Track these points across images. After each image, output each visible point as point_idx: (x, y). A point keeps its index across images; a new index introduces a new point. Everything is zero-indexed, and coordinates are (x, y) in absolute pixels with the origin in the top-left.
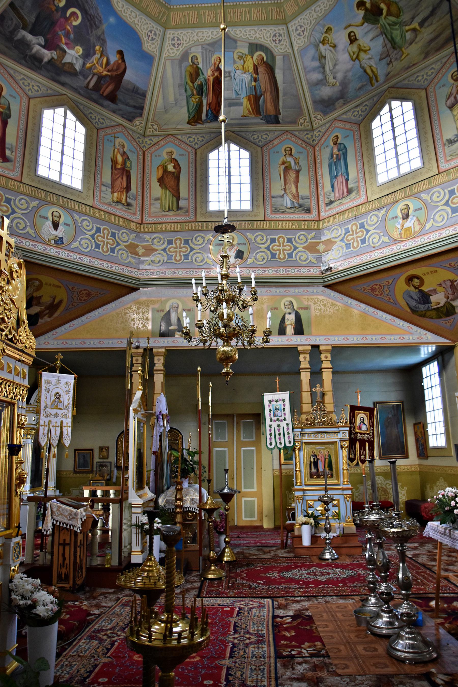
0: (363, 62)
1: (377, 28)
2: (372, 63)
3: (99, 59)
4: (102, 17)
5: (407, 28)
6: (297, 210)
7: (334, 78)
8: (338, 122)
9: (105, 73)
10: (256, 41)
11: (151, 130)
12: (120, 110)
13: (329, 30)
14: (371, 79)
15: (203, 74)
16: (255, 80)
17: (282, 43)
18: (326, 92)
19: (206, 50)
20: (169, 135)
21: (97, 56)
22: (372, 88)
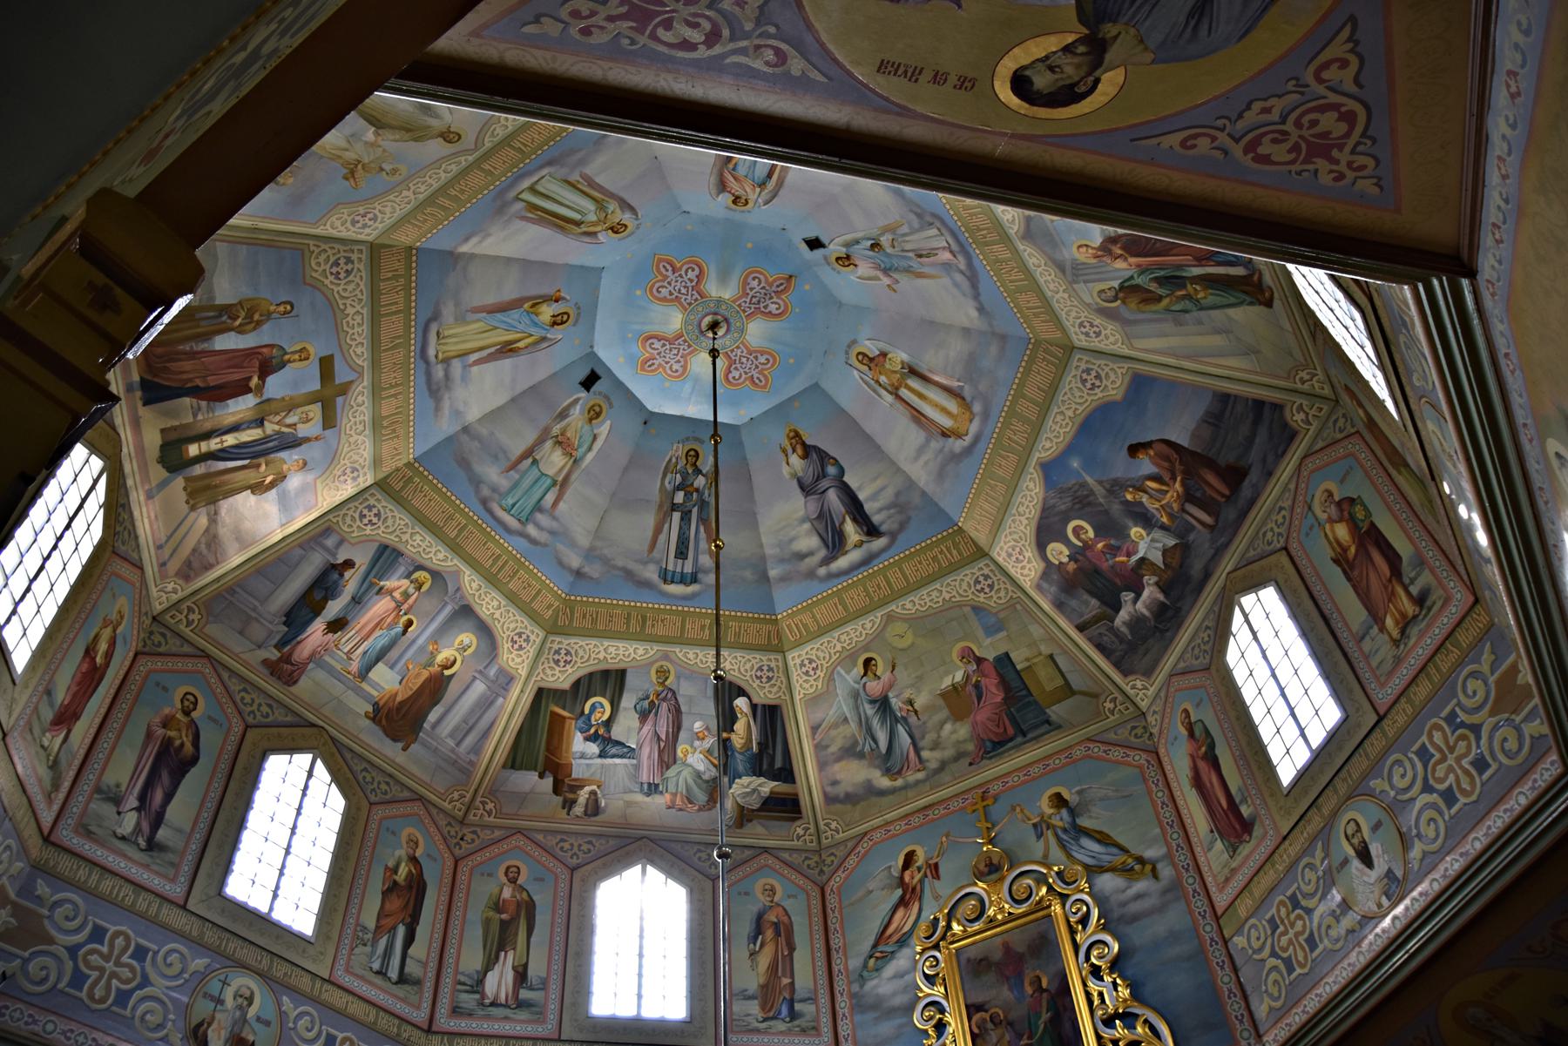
9: (1178, 485)
12: (1264, 461)
15: (1132, 278)
21: (1145, 499)
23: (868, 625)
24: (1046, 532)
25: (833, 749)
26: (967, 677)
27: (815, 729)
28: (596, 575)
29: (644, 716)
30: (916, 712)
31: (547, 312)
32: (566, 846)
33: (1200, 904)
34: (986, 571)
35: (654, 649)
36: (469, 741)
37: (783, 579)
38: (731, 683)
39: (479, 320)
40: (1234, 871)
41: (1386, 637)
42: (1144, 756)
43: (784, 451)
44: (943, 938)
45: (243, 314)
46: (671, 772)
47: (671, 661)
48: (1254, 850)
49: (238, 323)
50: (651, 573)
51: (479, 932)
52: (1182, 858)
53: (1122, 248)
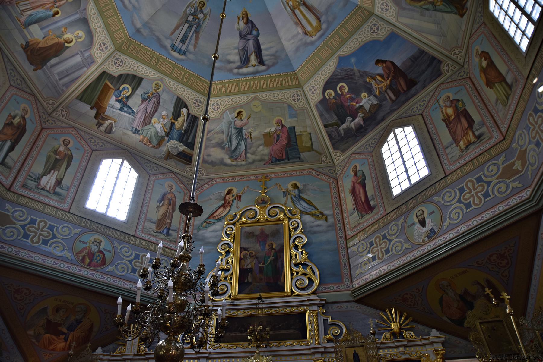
3: (376, 82)
4: (349, 67)
9: (388, 81)
11: (459, 57)
21: (373, 83)
23: (246, 98)
24: (330, 84)
25: (213, 142)
26: (276, 131)
28: (145, 34)
29: (144, 100)
30: (251, 138)
32: (93, 141)
33: (341, 234)
34: (299, 93)
35: (158, 75)
36: (66, 80)
40: (359, 224)
41: (458, 148)
42: (332, 180)
43: (239, 18)
44: (237, 222)
47: (163, 82)
48: (370, 218)
50: (168, 44)
51: (45, 159)
52: (338, 217)
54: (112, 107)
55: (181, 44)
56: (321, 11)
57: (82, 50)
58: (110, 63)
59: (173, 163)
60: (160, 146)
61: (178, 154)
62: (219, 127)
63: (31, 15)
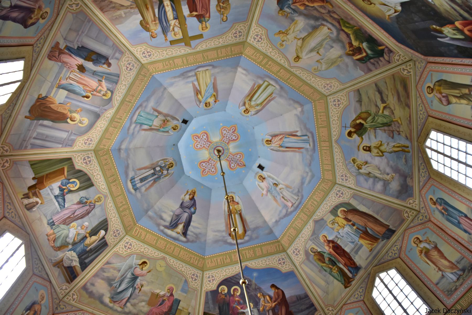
0: (388, 150)
1: (370, 131)
2: (392, 144)
3: (264, 300)
5: (381, 112)
6: (464, 276)
7: (388, 174)
8: (423, 191)
9: (274, 304)
10: (332, 207)
13: (354, 161)
14: (403, 151)
15: (325, 253)
16: (353, 225)
17: (344, 193)
18: (395, 186)
19: (313, 239)
20: (342, 307)
21: (262, 299)
22: (411, 153)
23: (156, 254)
24: (229, 282)
25: (106, 274)
26: (164, 296)
27: (108, 263)
28: (122, 156)
29: (80, 203)
30: (140, 290)
31: (211, 100)
35: (106, 191)
37: (150, 217)
38: (107, 224)
39: (211, 80)
43: (187, 192)
45: (224, 5)
46: (62, 226)
49: (221, 4)
50: (131, 174)
53: (333, 246)
54: (51, 190)
55: (139, 181)
56: (250, 227)
57: (74, 132)
58: (81, 156)
59: (57, 274)
60: (59, 250)
61: (68, 267)
62: (119, 264)
63: (71, 84)
